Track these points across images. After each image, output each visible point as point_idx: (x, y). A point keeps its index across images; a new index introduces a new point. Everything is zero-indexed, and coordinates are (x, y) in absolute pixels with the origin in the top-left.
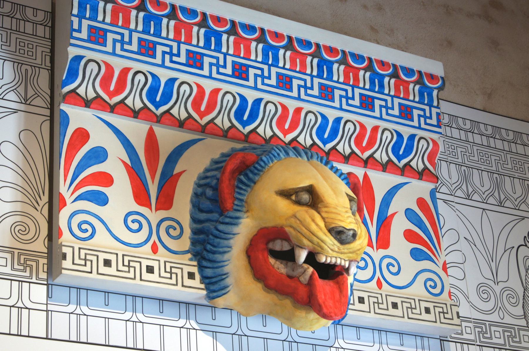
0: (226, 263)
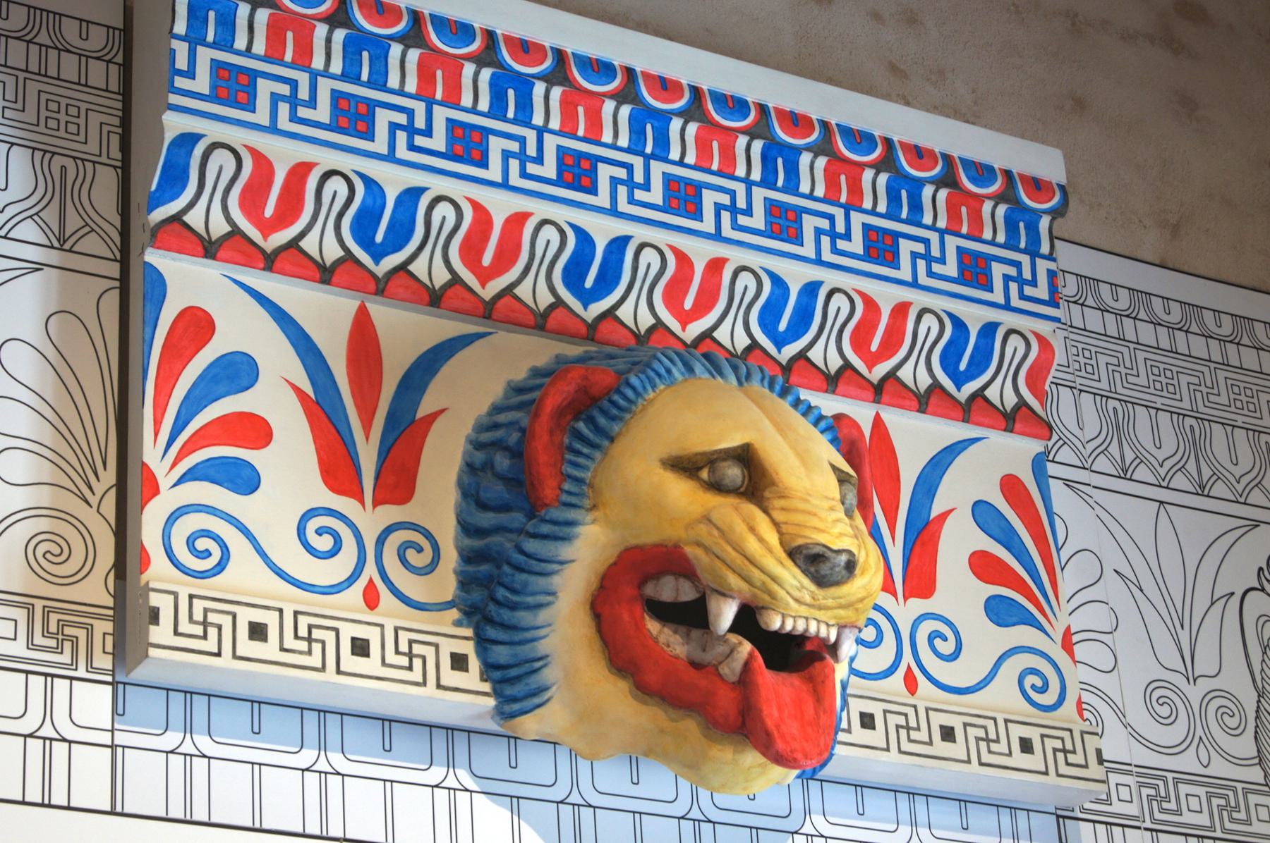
0: (542, 632)
